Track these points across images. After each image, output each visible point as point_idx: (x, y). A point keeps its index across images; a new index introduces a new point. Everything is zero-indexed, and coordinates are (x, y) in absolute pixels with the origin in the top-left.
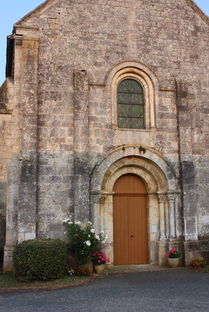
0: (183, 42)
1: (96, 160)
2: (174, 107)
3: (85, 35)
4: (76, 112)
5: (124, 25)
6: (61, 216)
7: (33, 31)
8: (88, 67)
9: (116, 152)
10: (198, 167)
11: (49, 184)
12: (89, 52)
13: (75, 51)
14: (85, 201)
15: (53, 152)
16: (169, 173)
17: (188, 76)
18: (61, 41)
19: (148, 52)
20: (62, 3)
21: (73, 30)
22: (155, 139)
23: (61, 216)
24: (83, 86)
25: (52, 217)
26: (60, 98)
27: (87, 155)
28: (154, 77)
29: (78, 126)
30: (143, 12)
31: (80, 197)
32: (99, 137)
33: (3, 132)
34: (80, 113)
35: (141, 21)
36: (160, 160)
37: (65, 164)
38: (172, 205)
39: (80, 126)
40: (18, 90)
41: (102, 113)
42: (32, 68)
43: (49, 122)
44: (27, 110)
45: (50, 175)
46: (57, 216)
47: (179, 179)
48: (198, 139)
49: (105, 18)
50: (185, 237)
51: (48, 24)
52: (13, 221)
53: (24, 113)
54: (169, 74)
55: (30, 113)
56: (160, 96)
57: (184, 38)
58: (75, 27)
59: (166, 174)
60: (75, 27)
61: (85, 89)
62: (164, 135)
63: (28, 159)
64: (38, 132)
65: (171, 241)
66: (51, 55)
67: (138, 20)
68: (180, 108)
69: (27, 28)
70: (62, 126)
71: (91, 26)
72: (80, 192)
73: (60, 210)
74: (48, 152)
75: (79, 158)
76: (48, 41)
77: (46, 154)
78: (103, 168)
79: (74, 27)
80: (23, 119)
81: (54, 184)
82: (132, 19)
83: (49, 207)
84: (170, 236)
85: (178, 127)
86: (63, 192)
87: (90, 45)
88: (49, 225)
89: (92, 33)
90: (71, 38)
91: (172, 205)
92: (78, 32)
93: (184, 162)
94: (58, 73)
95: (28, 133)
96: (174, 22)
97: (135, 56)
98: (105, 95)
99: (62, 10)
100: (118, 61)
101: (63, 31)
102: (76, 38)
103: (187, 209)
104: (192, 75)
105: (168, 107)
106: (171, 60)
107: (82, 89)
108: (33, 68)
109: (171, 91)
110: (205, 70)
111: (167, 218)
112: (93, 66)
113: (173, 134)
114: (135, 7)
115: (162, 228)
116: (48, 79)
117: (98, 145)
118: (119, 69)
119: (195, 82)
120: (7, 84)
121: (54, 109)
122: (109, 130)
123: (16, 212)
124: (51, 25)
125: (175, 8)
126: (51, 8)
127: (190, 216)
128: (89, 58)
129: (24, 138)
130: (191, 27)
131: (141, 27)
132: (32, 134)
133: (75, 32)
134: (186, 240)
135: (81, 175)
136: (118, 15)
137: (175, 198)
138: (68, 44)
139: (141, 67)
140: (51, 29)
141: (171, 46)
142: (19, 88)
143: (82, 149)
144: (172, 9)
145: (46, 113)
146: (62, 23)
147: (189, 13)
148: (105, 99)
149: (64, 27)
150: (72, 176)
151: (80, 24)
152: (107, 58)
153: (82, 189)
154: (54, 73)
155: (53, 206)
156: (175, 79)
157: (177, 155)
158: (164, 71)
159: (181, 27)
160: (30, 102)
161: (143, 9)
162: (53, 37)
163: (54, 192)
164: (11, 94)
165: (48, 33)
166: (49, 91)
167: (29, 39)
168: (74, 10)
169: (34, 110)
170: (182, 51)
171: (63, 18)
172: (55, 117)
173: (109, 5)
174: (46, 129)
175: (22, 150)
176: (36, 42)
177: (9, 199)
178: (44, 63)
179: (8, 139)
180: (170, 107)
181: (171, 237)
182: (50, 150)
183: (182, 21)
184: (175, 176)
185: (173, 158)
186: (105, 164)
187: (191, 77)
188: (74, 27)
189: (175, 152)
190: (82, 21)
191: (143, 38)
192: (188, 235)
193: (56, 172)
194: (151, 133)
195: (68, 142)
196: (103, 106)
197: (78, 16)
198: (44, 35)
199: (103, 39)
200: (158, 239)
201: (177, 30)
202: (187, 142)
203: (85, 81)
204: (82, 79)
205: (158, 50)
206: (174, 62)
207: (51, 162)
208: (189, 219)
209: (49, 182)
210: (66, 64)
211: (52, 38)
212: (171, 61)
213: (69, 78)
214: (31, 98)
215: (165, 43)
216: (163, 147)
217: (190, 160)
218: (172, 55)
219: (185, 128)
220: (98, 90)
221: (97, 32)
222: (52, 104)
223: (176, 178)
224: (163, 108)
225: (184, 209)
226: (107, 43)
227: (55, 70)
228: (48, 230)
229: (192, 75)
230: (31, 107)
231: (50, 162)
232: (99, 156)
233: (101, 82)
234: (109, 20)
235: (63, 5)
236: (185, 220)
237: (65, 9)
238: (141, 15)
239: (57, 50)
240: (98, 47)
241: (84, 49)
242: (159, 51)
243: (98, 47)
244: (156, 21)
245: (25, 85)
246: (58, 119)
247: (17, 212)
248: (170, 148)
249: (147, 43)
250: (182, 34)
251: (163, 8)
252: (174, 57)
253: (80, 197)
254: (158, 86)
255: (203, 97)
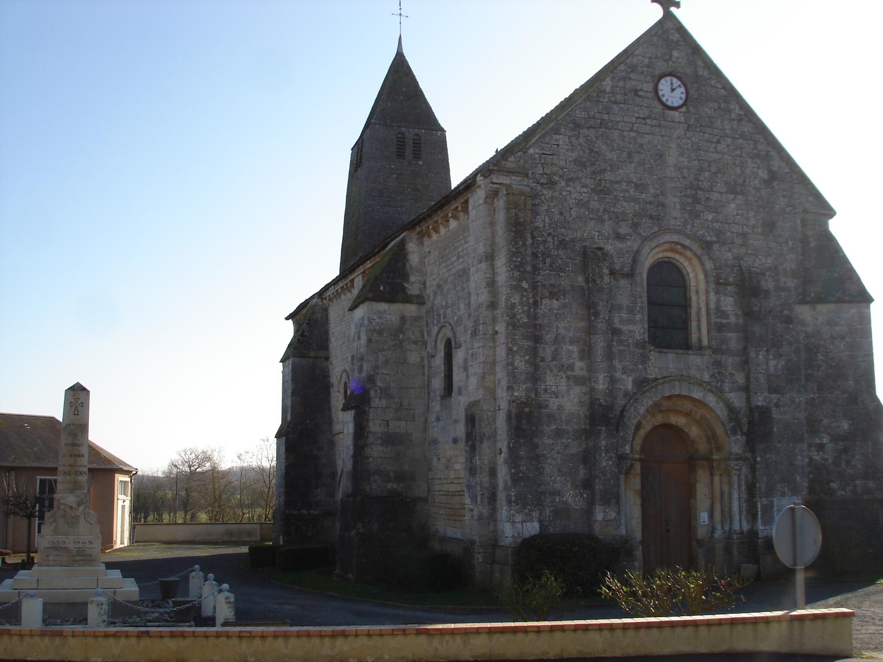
0: (751, 198)
1: (622, 402)
2: (738, 312)
3: (600, 186)
4: (593, 320)
5: (659, 167)
6: (571, 496)
7: (518, 177)
8: (606, 241)
9: (653, 388)
10: (775, 415)
11: (551, 441)
12: (607, 216)
13: (584, 213)
14: (612, 471)
15: (556, 387)
16: (731, 424)
17: (760, 259)
18: (562, 195)
19: (698, 216)
20: (562, 127)
21: (580, 176)
22: (711, 367)
23: (571, 496)
24: (601, 277)
25: (558, 497)
26: (564, 295)
27: (611, 393)
28: (707, 261)
29: (596, 346)
30: (688, 144)
31: (604, 464)
32: (627, 362)
33: (401, 337)
34: (599, 322)
35: (686, 160)
36: (719, 404)
37: (575, 408)
38: (735, 479)
39: (600, 343)
40: (489, 278)
41: (630, 322)
42: (523, 245)
43: (549, 337)
44: (518, 317)
45: (553, 427)
46: (564, 496)
47: (746, 434)
48: (776, 367)
49: (630, 155)
50: (758, 532)
51: (541, 165)
52: (489, 503)
53: (514, 322)
54: (729, 255)
55: (523, 322)
56: (717, 293)
57: (753, 192)
58: (584, 170)
59: (728, 427)
60: (584, 170)
61: (605, 281)
62: (724, 360)
63: (523, 399)
64: (534, 352)
65: (735, 538)
66: (547, 220)
67: (682, 159)
68: (749, 314)
69: (509, 172)
70: (568, 344)
71: (608, 168)
72: (604, 455)
73: (569, 486)
74: (549, 387)
75: (599, 399)
76: (543, 195)
77: (545, 390)
78: (632, 415)
79: (583, 171)
80: (512, 333)
81: (559, 441)
82: (672, 158)
83: (552, 481)
84: (732, 531)
85: (745, 349)
86: (573, 454)
87: (608, 203)
88: (552, 511)
89: (611, 182)
90: (578, 191)
91: (735, 479)
92: (589, 179)
93: (757, 407)
94: (560, 252)
95: (521, 356)
96: (737, 162)
97: (678, 223)
98: (634, 292)
99: (562, 140)
100: (653, 231)
101: (565, 177)
102: (585, 190)
103: (762, 485)
104: (766, 257)
105: (730, 312)
106: (733, 230)
107: (601, 281)
108: (524, 244)
109: (734, 284)
110: (785, 249)
111: (726, 499)
112: (613, 240)
113: (738, 359)
114: (676, 135)
115: (717, 516)
116: (545, 263)
117: (624, 377)
118: (654, 246)
119: (769, 269)
120: (407, 247)
121: (556, 314)
122: (641, 351)
123: (493, 488)
124: (545, 166)
125: (738, 138)
126: (543, 136)
127: (766, 497)
128: (608, 227)
129: (516, 364)
130: (763, 172)
131: (686, 171)
132: (526, 358)
133: (584, 179)
134: (760, 536)
135: (604, 428)
136: (650, 149)
137: (741, 468)
138: (574, 201)
139: (687, 243)
140: (546, 174)
141: (733, 206)
142: (491, 274)
143: (604, 384)
144: (734, 138)
145: (543, 321)
146: (562, 163)
147: (760, 147)
148: (634, 299)
149: (566, 170)
150: (585, 429)
151: (591, 166)
152: (635, 226)
153: (607, 451)
154: (554, 252)
155: (559, 478)
156: (740, 264)
157: (744, 396)
158: (723, 250)
159: (748, 171)
160: (522, 303)
161: (689, 139)
162: (549, 188)
163: (559, 455)
164: (413, 264)
165: (541, 181)
166: (547, 283)
167: (516, 192)
168: (582, 140)
169: (528, 316)
170: (750, 215)
171: (564, 153)
172: (557, 327)
173: (635, 132)
174: (544, 349)
175: (514, 385)
176: (528, 198)
177: (482, 465)
178: (538, 234)
179: (410, 350)
180: (733, 312)
181: (734, 532)
182: (551, 384)
183: (749, 160)
184: (741, 430)
185: (737, 399)
186: (636, 410)
187: (764, 260)
188: (583, 171)
189: (740, 389)
190: (593, 160)
191: (689, 192)
192: (763, 528)
193: (562, 421)
194: (705, 357)
195: (579, 371)
196: (631, 311)
197: (587, 151)
198: (536, 184)
199: (627, 193)
200: (709, 535)
201: (742, 177)
202: (760, 373)
203: (605, 268)
204: (600, 265)
205: (713, 212)
206: (738, 234)
207: (553, 404)
208: (765, 503)
209: (552, 438)
210: (572, 237)
211: (548, 190)
212: (733, 233)
213: (577, 261)
214: (523, 296)
215: (724, 200)
216: (723, 381)
217: (764, 404)
218: (734, 221)
219: (758, 350)
220: (623, 282)
221: (617, 180)
222: (552, 306)
223: (743, 434)
224: (723, 314)
225: (758, 485)
226: (636, 201)
227: (556, 247)
228: (551, 518)
229: (766, 257)
230: (524, 311)
231: (552, 404)
232: (626, 394)
233: (626, 269)
234: (636, 158)
235: (563, 130)
236: (759, 504)
237: (567, 137)
238: (685, 151)
239: (555, 211)
240: (619, 207)
241: (598, 211)
242: (713, 214)
243: (619, 207)
244: (708, 161)
245: (513, 274)
246: (563, 331)
247: (494, 488)
248: (733, 383)
249: (696, 201)
250: (750, 183)
251: (718, 137)
252: (737, 226)
253: (604, 464)
254: (714, 276)
255: (781, 296)
